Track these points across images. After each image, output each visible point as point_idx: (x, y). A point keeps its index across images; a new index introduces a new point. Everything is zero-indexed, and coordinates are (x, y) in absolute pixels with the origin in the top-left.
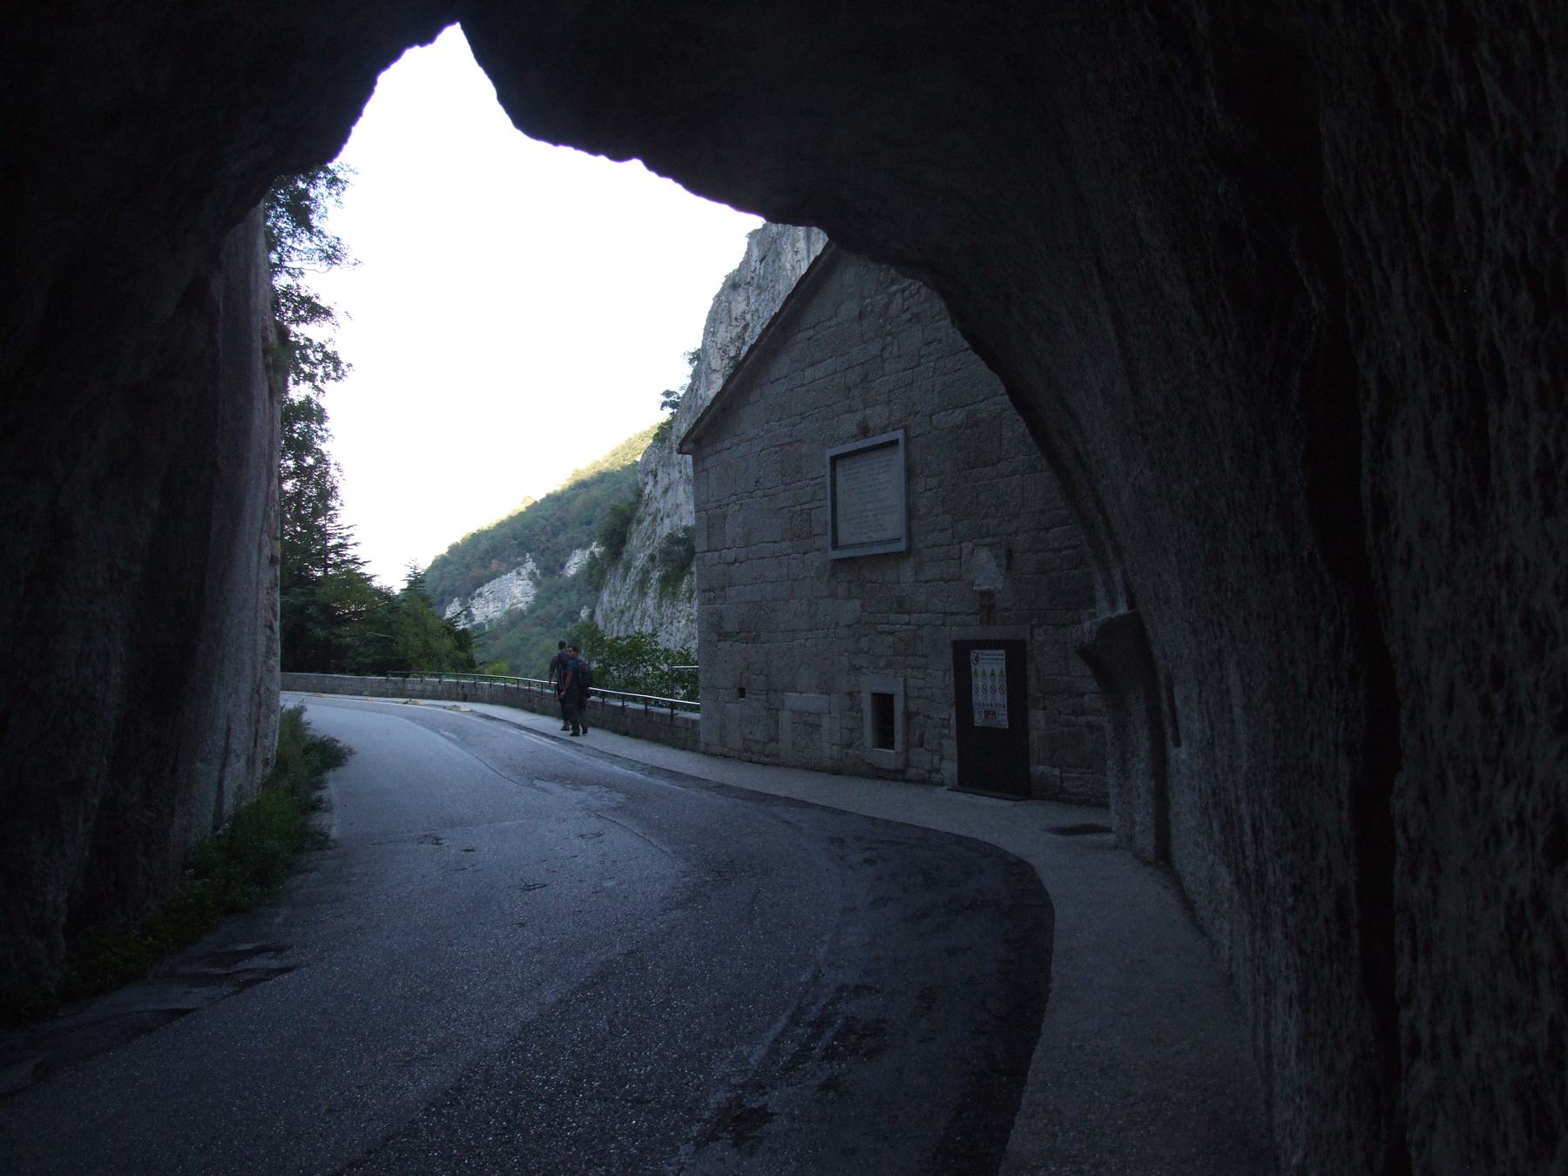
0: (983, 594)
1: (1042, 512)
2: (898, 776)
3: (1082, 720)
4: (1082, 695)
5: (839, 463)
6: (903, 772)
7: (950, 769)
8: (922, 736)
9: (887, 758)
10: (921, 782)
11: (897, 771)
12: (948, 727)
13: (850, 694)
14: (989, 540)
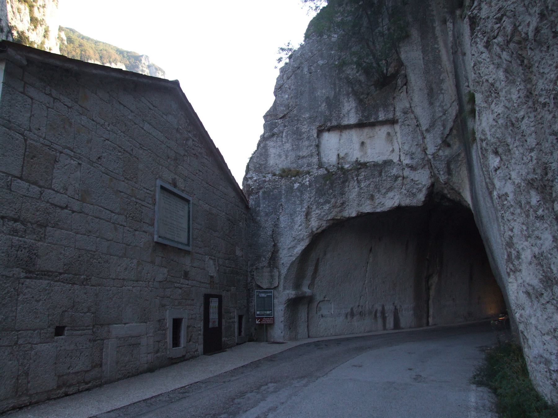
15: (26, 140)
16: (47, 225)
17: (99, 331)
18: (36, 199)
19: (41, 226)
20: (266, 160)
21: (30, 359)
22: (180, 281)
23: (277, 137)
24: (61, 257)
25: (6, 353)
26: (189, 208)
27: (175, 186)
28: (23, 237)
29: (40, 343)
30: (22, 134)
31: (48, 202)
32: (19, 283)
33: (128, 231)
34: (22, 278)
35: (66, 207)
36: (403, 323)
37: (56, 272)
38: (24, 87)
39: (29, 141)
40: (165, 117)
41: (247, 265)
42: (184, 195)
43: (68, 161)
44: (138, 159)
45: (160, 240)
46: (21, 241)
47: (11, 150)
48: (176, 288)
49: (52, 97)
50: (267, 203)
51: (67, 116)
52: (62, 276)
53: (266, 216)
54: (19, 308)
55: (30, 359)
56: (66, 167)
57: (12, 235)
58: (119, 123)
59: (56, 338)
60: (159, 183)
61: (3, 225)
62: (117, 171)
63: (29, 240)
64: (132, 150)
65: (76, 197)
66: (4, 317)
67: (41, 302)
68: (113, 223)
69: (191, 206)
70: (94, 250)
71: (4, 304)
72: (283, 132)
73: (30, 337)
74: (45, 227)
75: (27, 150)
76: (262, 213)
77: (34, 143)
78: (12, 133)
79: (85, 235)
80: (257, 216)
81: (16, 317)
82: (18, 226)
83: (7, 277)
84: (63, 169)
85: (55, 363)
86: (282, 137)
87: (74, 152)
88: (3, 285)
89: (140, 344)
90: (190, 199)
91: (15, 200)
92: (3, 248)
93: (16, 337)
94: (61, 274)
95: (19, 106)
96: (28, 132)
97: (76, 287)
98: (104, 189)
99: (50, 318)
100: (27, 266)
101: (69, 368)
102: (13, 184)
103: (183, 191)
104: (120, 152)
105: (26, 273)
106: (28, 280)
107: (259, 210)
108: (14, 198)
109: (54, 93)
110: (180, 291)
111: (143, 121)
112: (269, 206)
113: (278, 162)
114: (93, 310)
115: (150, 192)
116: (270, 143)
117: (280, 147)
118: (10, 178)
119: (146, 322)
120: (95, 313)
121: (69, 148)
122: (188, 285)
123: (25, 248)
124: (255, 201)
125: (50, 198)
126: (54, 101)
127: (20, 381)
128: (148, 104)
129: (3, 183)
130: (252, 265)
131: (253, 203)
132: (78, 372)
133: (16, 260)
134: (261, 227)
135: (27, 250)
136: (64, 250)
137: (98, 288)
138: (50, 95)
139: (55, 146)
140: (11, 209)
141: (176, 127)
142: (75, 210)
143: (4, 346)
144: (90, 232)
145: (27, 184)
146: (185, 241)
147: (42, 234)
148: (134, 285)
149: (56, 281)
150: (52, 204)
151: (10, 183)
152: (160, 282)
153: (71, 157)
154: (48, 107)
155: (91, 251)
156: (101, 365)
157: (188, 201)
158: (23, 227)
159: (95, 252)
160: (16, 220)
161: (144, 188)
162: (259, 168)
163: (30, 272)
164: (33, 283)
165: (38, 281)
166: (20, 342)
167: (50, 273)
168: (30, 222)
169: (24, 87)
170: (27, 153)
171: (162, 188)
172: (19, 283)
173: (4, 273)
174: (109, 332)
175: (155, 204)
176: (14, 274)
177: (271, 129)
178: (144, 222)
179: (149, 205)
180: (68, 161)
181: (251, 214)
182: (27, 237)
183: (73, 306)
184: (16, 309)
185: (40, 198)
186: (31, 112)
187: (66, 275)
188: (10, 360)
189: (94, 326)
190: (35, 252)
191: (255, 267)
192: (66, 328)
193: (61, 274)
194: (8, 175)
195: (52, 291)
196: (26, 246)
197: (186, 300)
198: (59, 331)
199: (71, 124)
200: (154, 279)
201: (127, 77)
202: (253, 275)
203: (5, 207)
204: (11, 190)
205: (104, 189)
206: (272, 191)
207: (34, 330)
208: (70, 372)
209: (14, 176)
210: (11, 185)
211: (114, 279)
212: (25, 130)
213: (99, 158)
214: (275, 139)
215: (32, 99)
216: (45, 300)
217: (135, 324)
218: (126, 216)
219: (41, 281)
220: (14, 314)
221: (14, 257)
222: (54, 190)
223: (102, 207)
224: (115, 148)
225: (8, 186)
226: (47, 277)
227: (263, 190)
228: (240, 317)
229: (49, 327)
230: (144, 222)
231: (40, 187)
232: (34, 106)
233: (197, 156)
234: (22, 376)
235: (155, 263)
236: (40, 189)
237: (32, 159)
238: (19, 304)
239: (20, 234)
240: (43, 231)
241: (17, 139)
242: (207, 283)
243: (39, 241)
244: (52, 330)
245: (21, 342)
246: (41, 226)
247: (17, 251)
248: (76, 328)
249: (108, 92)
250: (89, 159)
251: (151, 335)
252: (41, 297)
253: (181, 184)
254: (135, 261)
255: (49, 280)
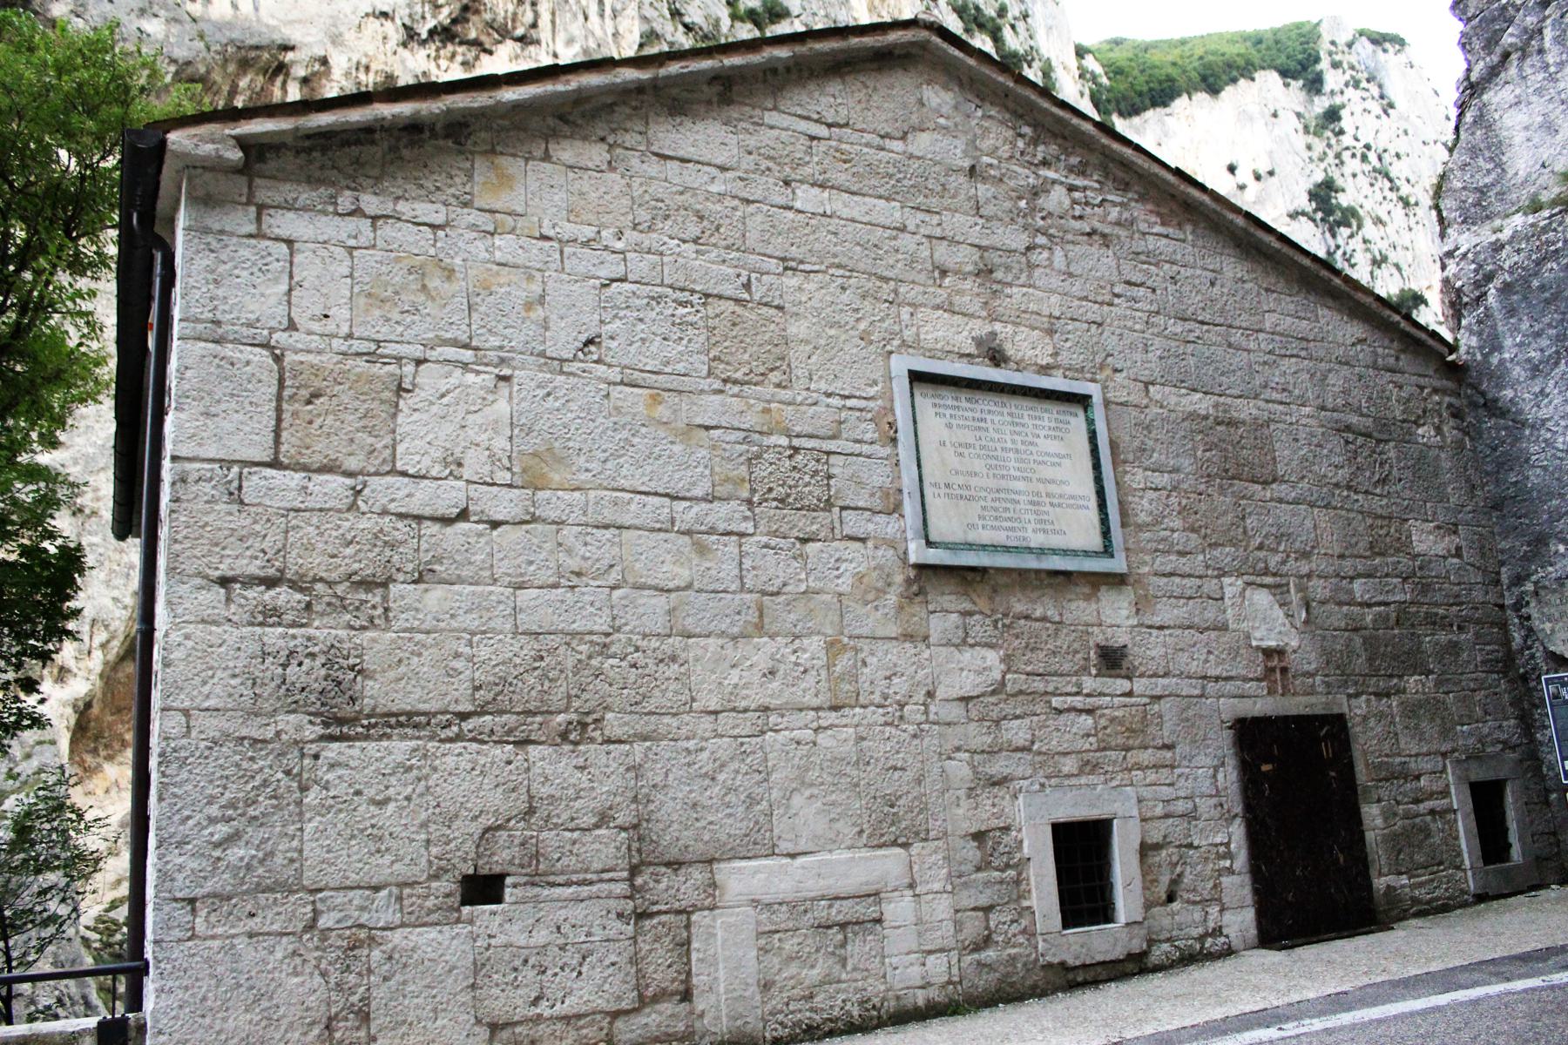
0: (1268, 653)
1: (1342, 556)
2: (1134, 966)
3: (1424, 807)
4: (1418, 778)
5: (932, 538)
6: (1144, 954)
7: (1241, 921)
8: (1176, 882)
9: (1099, 942)
10: (1189, 959)
11: (1131, 957)
12: (1229, 855)
13: (979, 837)
14: (1268, 580)
15: (278, 359)
16: (390, 579)
17: (662, 886)
18: (339, 511)
19: (367, 584)
20: (1499, 165)
21: (370, 971)
22: (1079, 685)
23: (1523, 58)
24: (459, 664)
25: (279, 955)
26: (1090, 422)
27: (997, 357)
28: (302, 625)
29: (403, 925)
30: (265, 346)
31: (384, 512)
32: (303, 756)
33: (766, 546)
34: (312, 742)
35: (463, 515)
36: (620, 1024)
37: (445, 712)
38: (259, 219)
39: (290, 358)
40: (897, 145)
41: (1498, 582)
42: (1056, 383)
43: (453, 381)
44: (780, 308)
45: (935, 556)
46: (294, 637)
47: (232, 395)
48: (1059, 712)
49: (366, 216)
50: (1525, 326)
51: (432, 252)
52: (467, 725)
53: (1533, 378)
54: (309, 827)
55: (370, 971)
56: (445, 400)
57: (261, 624)
58: (667, 217)
59: (466, 910)
60: (901, 365)
61: (228, 600)
62: (680, 367)
63: (325, 630)
64: (747, 286)
65: (503, 477)
66: (261, 855)
67: (391, 807)
68: (688, 533)
69: (1098, 413)
70: (605, 628)
71: (255, 818)
72: (1540, 31)
73: (362, 909)
74: (385, 585)
75: (288, 383)
76: (1517, 372)
77: (310, 358)
78: (228, 350)
79: (555, 586)
80: (1501, 387)
81: (301, 851)
82: (283, 596)
83: (256, 741)
84: (434, 409)
85: (473, 986)
86: (1541, 51)
87: (476, 349)
88: (245, 765)
89: (879, 921)
90: (1092, 389)
91: (258, 527)
92: (231, 664)
93: (309, 908)
94: (464, 716)
95: (245, 273)
96: (286, 335)
97: (534, 751)
98: (625, 434)
99: (434, 850)
100: (323, 704)
101: (536, 1002)
102: (245, 484)
103: (1045, 370)
104: (683, 304)
105: (326, 725)
106: (335, 745)
107: (1502, 362)
108: (255, 522)
109: (371, 203)
110: (1087, 721)
111: (787, 183)
112: (1538, 335)
113: (1545, 154)
114: (623, 818)
115: (862, 404)
116: (1497, 97)
117: (1539, 92)
118: (235, 469)
119: (905, 846)
120: (635, 827)
121: (455, 343)
122: (1130, 694)
123: (312, 655)
124: (1480, 334)
125: (393, 500)
126: (373, 225)
127: (338, 1035)
128: (803, 126)
129: (214, 487)
130: (1518, 580)
131: (1474, 341)
132: (579, 1016)
133: (282, 691)
134: (1524, 424)
135: (321, 659)
136: (470, 644)
137: (639, 748)
138: (357, 212)
139: (390, 349)
140: (248, 553)
141: (967, 164)
142: (499, 517)
143: (268, 934)
144: (579, 574)
145: (299, 476)
146: (1096, 542)
147: (374, 607)
148: (823, 723)
149: (451, 740)
150: (401, 516)
151: (235, 484)
152: (965, 700)
153: (465, 366)
154: (351, 250)
155: (591, 633)
156: (686, 996)
157: (1083, 401)
158: (298, 596)
159: (608, 635)
160: (270, 583)
161: (829, 395)
162: (1477, 204)
163: (341, 722)
164: (356, 752)
165: (371, 746)
166: (323, 922)
167: (423, 719)
168: (321, 580)
169: (259, 219)
170: (286, 393)
171: (916, 377)
172: (303, 756)
173: (244, 732)
174: (714, 885)
175: (894, 440)
176: (278, 734)
177: (1491, 43)
178: (843, 508)
179: (865, 449)
180: (453, 381)
181: (1474, 387)
182: (316, 623)
183: (531, 811)
184: (301, 829)
185: (352, 507)
186: (291, 277)
187: (488, 718)
188: (296, 974)
189: (634, 871)
190: (352, 661)
191: (1530, 587)
192: (509, 880)
193: (464, 716)
194: (226, 463)
195: (435, 769)
196: (316, 649)
197: (1128, 749)
198: (483, 888)
199: (450, 273)
200: (930, 694)
201: (662, 72)
202: (1529, 618)
203: (228, 552)
204: (242, 502)
205: (625, 434)
206: (1536, 274)
207: (377, 889)
208: (540, 1016)
209: (245, 463)
210: (240, 488)
211: (716, 713)
212: (272, 330)
213: (590, 342)
214: (1513, 71)
215: (289, 242)
216: (408, 798)
217: (847, 855)
218: (749, 502)
219: (385, 743)
220: (295, 843)
221: (273, 684)
222: (404, 474)
223: (623, 490)
224: (658, 299)
225: (231, 494)
226: (409, 731)
227: (1497, 282)
228: (1487, 799)
229: (436, 877)
230: (843, 508)
231: (350, 474)
232: (298, 259)
233: (1104, 236)
234: (346, 1019)
235: (926, 638)
236: (349, 482)
237: (309, 402)
238: (308, 815)
239: (288, 618)
240: (378, 599)
241: (248, 363)
242: (1246, 680)
243: (363, 628)
244: (447, 885)
245: (330, 924)
246: (367, 584)
247: (285, 666)
248: (551, 879)
249: (603, 139)
250: (542, 354)
251: (937, 886)
252: (391, 791)
253: (1026, 345)
254: (815, 644)
255: (419, 738)
